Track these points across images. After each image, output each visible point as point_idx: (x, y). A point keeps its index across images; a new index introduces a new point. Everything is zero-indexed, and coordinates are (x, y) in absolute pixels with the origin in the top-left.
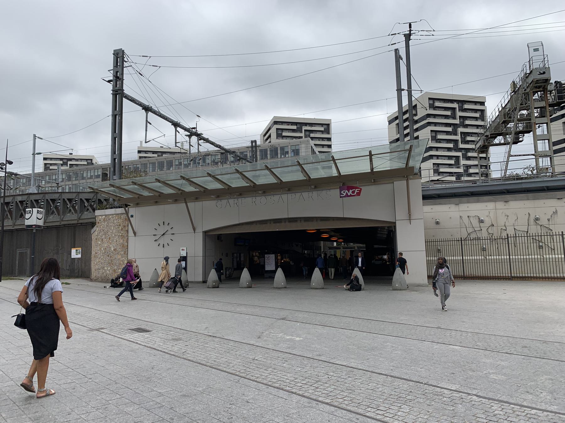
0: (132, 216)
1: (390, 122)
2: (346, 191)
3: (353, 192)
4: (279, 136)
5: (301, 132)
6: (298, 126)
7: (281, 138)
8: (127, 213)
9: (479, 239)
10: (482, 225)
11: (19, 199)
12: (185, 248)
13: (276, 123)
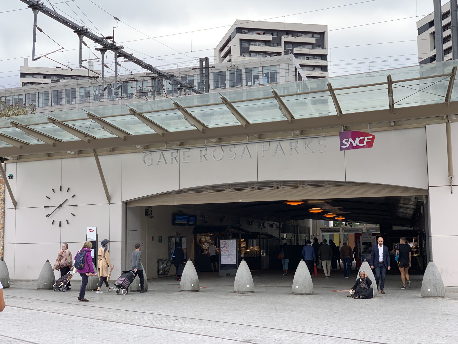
0: (11, 177)
1: (421, 30)
2: (351, 140)
3: (361, 141)
4: (244, 51)
6: (275, 35)
7: (247, 55)
12: (94, 229)
13: (239, 30)
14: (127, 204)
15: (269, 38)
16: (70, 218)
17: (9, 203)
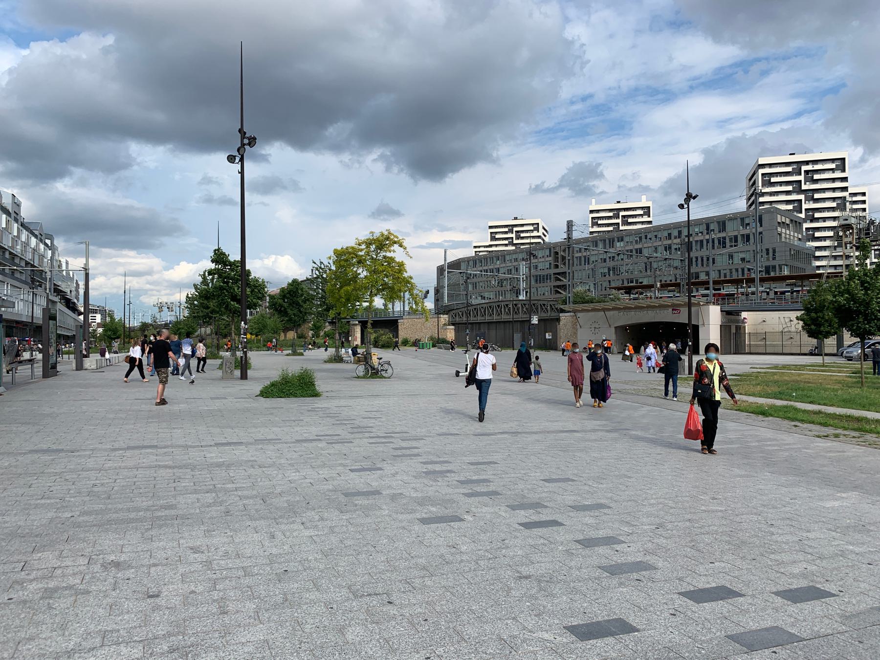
15: (506, 230)
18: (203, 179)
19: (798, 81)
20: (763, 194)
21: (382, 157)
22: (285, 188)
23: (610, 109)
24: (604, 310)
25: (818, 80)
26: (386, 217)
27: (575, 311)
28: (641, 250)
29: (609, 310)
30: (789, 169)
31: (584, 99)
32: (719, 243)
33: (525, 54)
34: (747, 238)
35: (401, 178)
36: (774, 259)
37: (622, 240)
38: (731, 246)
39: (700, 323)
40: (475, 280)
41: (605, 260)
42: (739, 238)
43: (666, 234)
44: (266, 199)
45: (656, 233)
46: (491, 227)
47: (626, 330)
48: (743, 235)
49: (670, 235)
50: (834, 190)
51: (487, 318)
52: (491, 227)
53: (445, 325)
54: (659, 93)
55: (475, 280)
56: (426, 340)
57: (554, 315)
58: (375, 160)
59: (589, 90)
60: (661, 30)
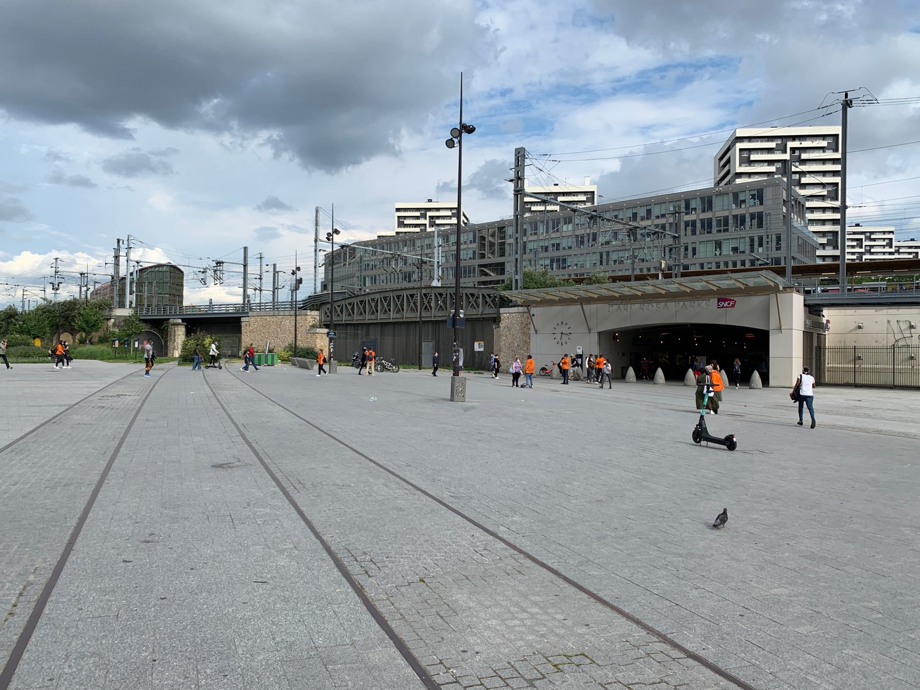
5: (785, 152)
6: (779, 142)
8: (529, 312)
9: (908, 346)
10: (913, 330)
11: (424, 291)
14: (599, 333)
15: (418, 214)
16: (554, 336)
17: (532, 331)
18: (49, 155)
19: (721, 91)
20: (739, 175)
21: (270, 140)
22: (153, 169)
23: (530, 107)
24: (582, 301)
25: (740, 92)
26: (275, 210)
27: (527, 304)
28: (595, 235)
29: (590, 300)
30: (772, 145)
31: (504, 93)
32: (703, 227)
33: (435, 36)
34: (740, 221)
35: (290, 163)
36: (778, 249)
37: (570, 222)
38: (719, 231)
39: (773, 325)
40: (374, 272)
41: (547, 248)
42: (731, 221)
43: (629, 214)
44: (132, 182)
45: (615, 213)
46: (398, 210)
47: (615, 338)
48: (735, 217)
49: (635, 215)
50: (824, 173)
51: (380, 317)
52: (398, 210)
53: (313, 326)
54: (584, 94)
55: (374, 272)
56: (279, 350)
57: (489, 311)
58: (261, 145)
59: (508, 84)
60: (584, 26)
